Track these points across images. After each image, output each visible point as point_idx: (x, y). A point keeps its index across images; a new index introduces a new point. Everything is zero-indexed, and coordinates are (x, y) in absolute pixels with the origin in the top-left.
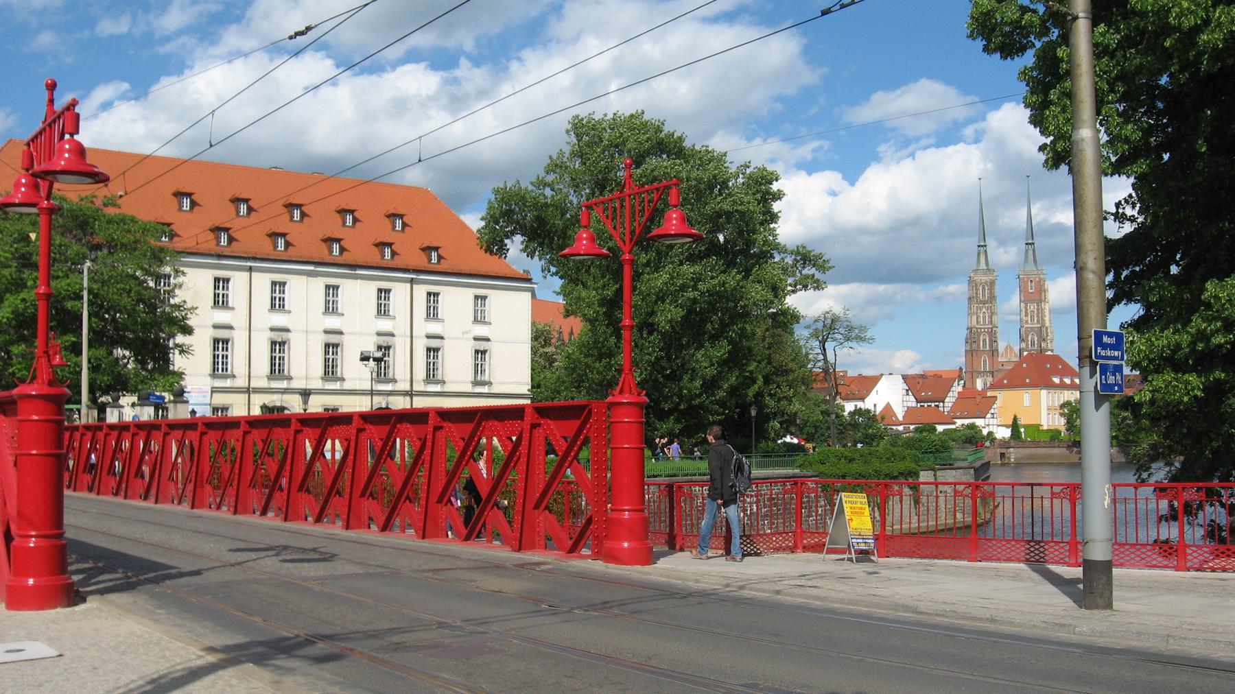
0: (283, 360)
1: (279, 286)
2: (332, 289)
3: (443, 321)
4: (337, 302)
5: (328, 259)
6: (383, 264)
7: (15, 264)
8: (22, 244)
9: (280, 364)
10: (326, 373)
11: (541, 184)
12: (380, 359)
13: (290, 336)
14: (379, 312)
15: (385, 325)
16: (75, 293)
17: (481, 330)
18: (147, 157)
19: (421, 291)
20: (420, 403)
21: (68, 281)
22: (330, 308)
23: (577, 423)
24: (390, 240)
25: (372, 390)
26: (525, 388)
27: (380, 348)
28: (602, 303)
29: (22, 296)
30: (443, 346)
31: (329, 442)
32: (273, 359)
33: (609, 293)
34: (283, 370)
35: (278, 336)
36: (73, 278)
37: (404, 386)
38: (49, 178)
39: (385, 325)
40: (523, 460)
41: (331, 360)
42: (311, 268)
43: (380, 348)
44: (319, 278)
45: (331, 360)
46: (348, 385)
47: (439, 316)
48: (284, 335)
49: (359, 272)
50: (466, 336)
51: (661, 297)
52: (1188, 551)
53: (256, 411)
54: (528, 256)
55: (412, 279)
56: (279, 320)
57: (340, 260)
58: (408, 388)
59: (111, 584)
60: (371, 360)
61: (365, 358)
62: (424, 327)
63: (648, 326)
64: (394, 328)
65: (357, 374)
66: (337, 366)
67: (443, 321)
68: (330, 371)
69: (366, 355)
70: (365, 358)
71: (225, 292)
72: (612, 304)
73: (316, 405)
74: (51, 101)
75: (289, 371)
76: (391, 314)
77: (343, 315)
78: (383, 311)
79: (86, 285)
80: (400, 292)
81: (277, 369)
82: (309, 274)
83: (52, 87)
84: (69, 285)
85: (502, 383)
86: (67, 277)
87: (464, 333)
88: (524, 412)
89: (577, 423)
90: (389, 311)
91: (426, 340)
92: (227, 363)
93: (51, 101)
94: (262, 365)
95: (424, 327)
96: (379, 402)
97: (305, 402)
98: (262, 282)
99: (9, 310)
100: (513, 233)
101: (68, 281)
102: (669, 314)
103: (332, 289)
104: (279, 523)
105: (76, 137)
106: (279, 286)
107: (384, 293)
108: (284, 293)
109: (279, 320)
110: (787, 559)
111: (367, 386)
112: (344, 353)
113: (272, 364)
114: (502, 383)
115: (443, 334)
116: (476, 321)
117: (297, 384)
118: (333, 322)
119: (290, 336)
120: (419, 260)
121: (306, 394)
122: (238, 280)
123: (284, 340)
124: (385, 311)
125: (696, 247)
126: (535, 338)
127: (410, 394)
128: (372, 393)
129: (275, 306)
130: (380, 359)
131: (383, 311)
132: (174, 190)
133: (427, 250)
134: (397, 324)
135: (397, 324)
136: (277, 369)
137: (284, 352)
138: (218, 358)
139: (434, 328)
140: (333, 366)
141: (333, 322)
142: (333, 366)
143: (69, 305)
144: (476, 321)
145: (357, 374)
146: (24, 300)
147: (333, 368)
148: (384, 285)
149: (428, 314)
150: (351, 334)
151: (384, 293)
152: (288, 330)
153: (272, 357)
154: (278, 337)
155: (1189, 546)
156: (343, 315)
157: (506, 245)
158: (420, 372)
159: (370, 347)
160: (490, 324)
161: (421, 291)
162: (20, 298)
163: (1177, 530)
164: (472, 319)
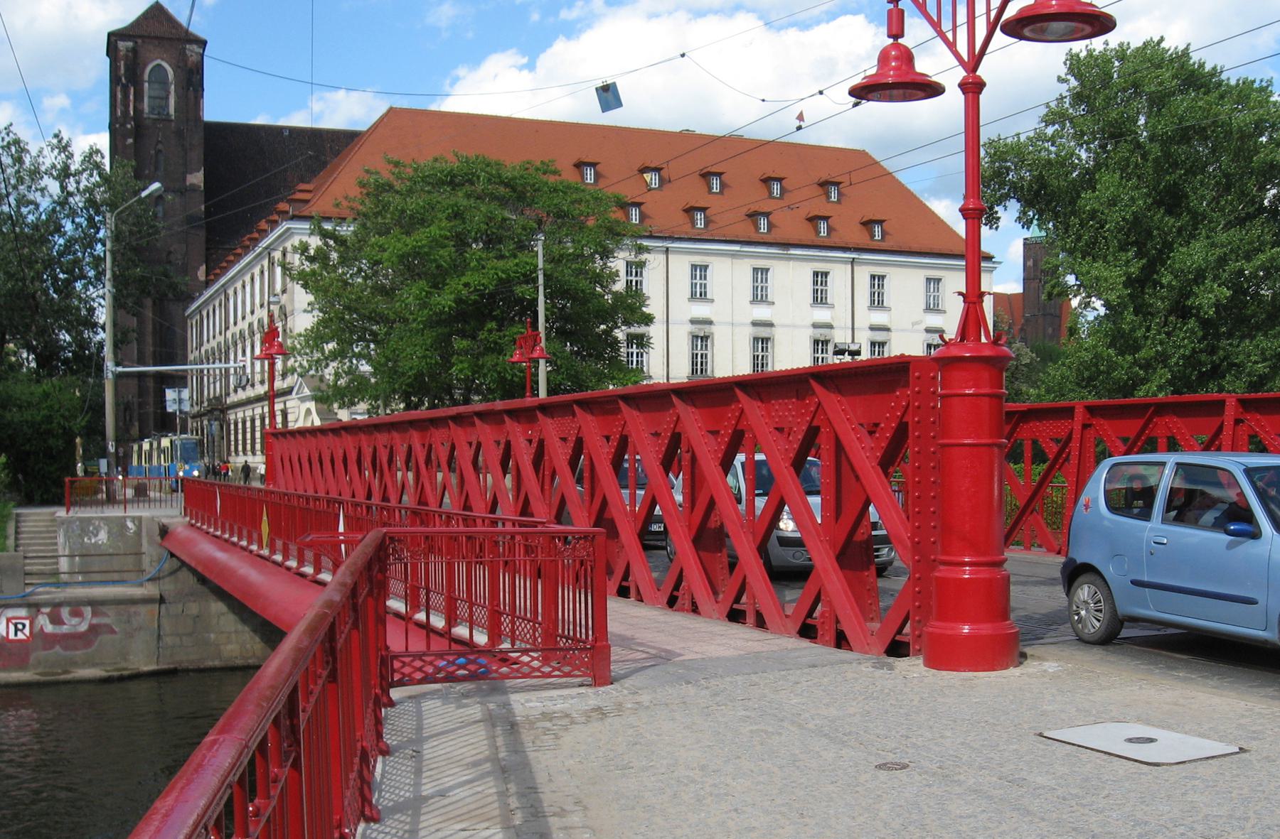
0: (706, 358)
1: (699, 271)
2: (760, 273)
3: (889, 309)
4: (767, 288)
5: (755, 237)
6: (818, 242)
7: (452, 243)
8: (457, 222)
9: (702, 363)
11: (1040, 137)
13: (714, 329)
14: (815, 299)
15: (822, 315)
16: (524, 275)
17: (762, 313)
19: (863, 274)
21: (517, 261)
22: (759, 297)
23: (1140, 423)
24: (827, 214)
28: (1129, 282)
29: (464, 280)
30: (890, 340)
32: (694, 356)
33: (1134, 270)
34: (706, 370)
35: (700, 329)
36: (523, 257)
39: (822, 315)
40: (1074, 461)
41: (760, 358)
42: (736, 248)
44: (747, 260)
45: (760, 358)
47: (885, 304)
48: (707, 328)
49: (793, 251)
51: (1200, 277)
52: (397, 664)
54: (1023, 227)
55: (854, 259)
56: (701, 310)
57: (769, 239)
59: (571, 587)
60: (847, 353)
63: (1182, 311)
64: (832, 318)
66: (767, 364)
67: (889, 309)
69: (842, 347)
71: (639, 279)
72: (1139, 284)
75: (713, 371)
76: (829, 301)
77: (773, 303)
78: (819, 298)
79: (541, 265)
80: (839, 276)
82: (734, 255)
84: (517, 265)
86: (515, 256)
87: (914, 324)
88: (743, 435)
89: (1140, 423)
90: (826, 298)
91: (870, 332)
92: (642, 361)
98: (681, 265)
99: (453, 296)
100: (1006, 197)
101: (517, 261)
102: (1210, 296)
103: (760, 273)
106: (699, 271)
107: (820, 277)
108: (705, 279)
109: (701, 310)
112: (776, 350)
115: (889, 326)
116: (928, 309)
119: (714, 329)
120: (860, 237)
123: (707, 334)
124: (822, 298)
125: (1243, 209)
129: (696, 295)
131: (819, 298)
132: (574, 161)
133: (868, 224)
137: (706, 349)
138: (632, 356)
139: (879, 318)
140: (763, 364)
142: (763, 364)
143: (519, 290)
144: (928, 309)
146: (466, 285)
147: (763, 367)
148: (821, 267)
149: (873, 302)
150: (783, 326)
151: (820, 277)
152: (711, 323)
153: (693, 354)
154: (700, 330)
155: (396, 657)
156: (773, 303)
157: (997, 212)
160: (945, 312)
161: (863, 274)
162: (462, 282)
163: (609, 629)
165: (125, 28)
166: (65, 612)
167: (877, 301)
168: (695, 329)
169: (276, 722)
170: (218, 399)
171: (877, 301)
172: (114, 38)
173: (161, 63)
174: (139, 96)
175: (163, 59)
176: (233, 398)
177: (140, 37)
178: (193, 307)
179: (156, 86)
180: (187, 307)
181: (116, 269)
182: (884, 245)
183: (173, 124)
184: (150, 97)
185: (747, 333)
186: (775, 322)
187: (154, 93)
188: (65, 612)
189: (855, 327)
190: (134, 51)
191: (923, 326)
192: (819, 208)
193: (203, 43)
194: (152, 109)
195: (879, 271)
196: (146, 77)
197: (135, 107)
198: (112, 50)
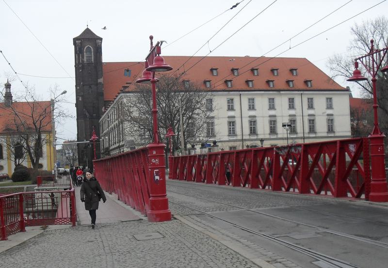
5: (269, 89)
10: (329, 130)
12: (291, 126)
15: (292, 112)
18: (204, 57)
20: (307, 141)
25: (304, 139)
26: (349, 134)
27: (291, 121)
31: (266, 158)
32: (251, 128)
37: (301, 135)
38: (153, 70)
39: (292, 112)
43: (291, 121)
46: (280, 136)
49: (281, 92)
50: (324, 114)
53: (245, 148)
56: (252, 113)
58: (302, 136)
61: (284, 126)
62: (235, 113)
65: (282, 132)
68: (273, 131)
69: (285, 124)
70: (284, 126)
73: (267, 144)
74: (152, 43)
81: (253, 131)
82: (262, 95)
83: (151, 38)
85: (339, 132)
87: (323, 113)
93: (152, 43)
94: (247, 131)
95: (235, 113)
96: (290, 142)
97: (262, 144)
104: (232, 188)
105: (160, 55)
107: (231, 101)
109: (252, 113)
110: (23, 245)
111: (285, 136)
113: (251, 130)
114: (339, 132)
117: (260, 137)
118: (272, 112)
120: (302, 86)
121: (262, 140)
122: (237, 100)
126: (352, 114)
127: (304, 138)
128: (287, 139)
130: (291, 126)
133: (306, 82)
134: (297, 112)
135: (297, 112)
136: (253, 131)
141: (272, 112)
145: (282, 132)
148: (291, 97)
149: (309, 107)
150: (259, 117)
151: (231, 101)
158: (307, 130)
159: (286, 121)
164: (288, 107)
165: (80, 36)
166: (36, 215)
167: (311, 107)
168: (250, 119)
169: (271, 264)
170: (108, 149)
171: (311, 107)
172: (75, 40)
173: (88, 46)
174: (83, 57)
175: (90, 45)
176: (111, 148)
177: (83, 39)
178: (101, 119)
179: (88, 53)
180: (99, 120)
181: (103, 109)
182: (311, 89)
183: (93, 65)
184: (86, 57)
185: (226, 121)
186: (277, 115)
187: (87, 56)
188: (36, 215)
189: (304, 115)
190: (81, 43)
191: (326, 114)
192: (290, 78)
193: (101, 39)
194: (87, 60)
195: (310, 97)
196: (85, 51)
197: (82, 60)
198: (75, 44)
